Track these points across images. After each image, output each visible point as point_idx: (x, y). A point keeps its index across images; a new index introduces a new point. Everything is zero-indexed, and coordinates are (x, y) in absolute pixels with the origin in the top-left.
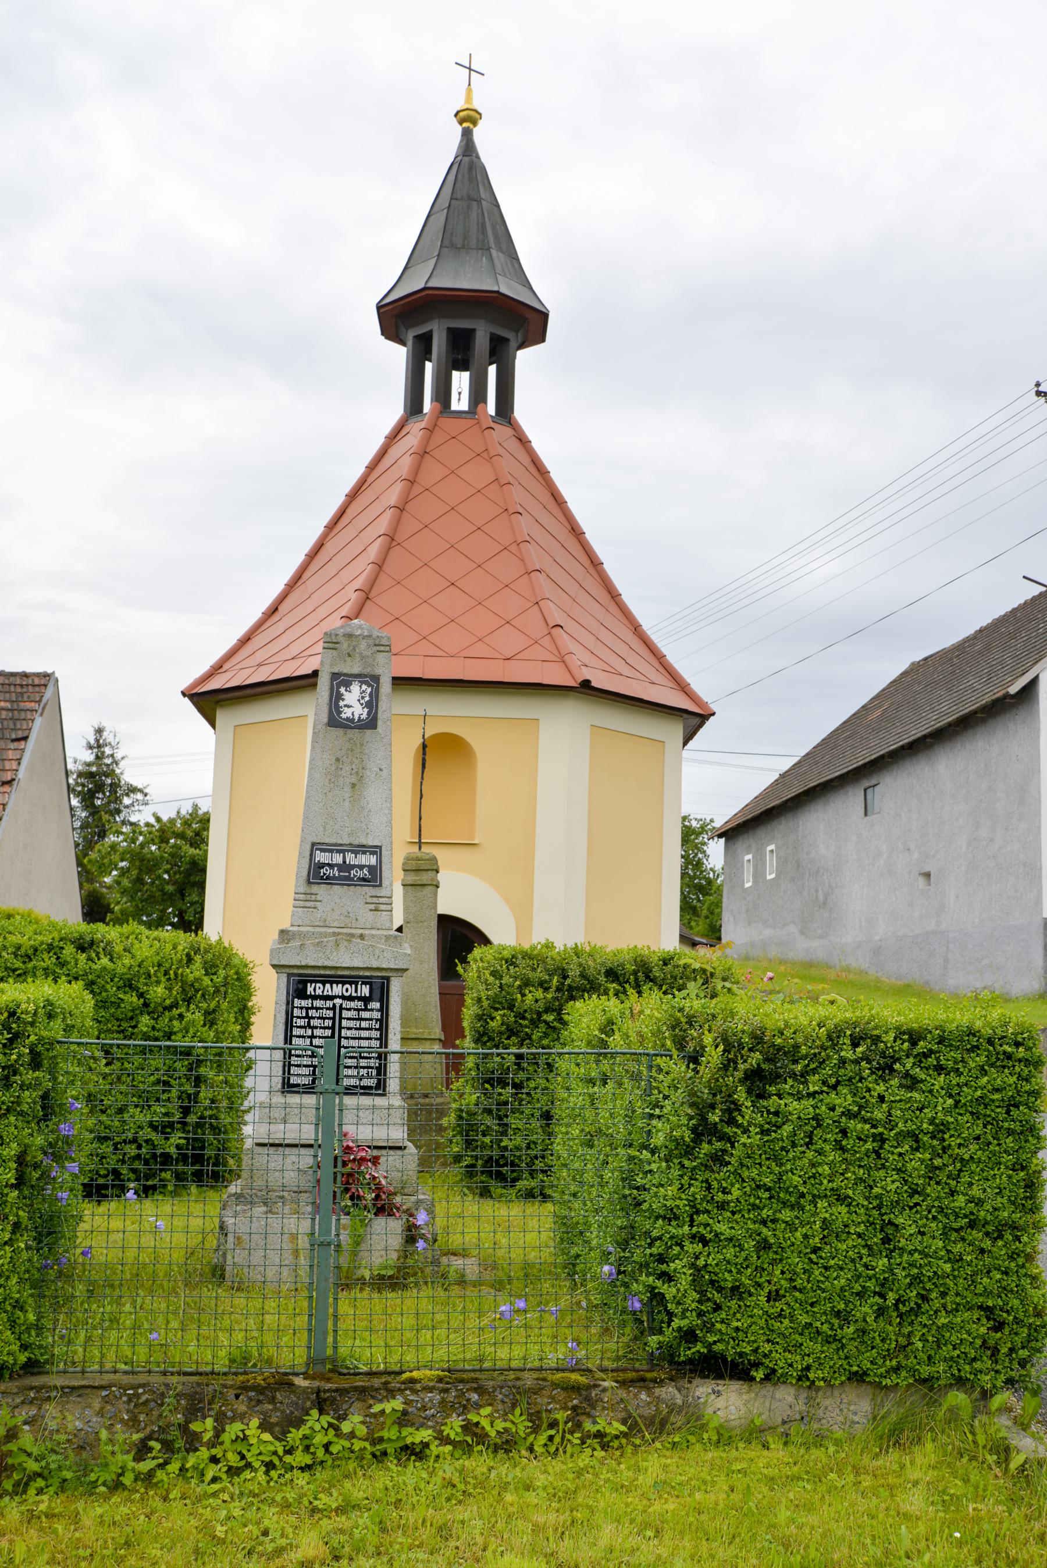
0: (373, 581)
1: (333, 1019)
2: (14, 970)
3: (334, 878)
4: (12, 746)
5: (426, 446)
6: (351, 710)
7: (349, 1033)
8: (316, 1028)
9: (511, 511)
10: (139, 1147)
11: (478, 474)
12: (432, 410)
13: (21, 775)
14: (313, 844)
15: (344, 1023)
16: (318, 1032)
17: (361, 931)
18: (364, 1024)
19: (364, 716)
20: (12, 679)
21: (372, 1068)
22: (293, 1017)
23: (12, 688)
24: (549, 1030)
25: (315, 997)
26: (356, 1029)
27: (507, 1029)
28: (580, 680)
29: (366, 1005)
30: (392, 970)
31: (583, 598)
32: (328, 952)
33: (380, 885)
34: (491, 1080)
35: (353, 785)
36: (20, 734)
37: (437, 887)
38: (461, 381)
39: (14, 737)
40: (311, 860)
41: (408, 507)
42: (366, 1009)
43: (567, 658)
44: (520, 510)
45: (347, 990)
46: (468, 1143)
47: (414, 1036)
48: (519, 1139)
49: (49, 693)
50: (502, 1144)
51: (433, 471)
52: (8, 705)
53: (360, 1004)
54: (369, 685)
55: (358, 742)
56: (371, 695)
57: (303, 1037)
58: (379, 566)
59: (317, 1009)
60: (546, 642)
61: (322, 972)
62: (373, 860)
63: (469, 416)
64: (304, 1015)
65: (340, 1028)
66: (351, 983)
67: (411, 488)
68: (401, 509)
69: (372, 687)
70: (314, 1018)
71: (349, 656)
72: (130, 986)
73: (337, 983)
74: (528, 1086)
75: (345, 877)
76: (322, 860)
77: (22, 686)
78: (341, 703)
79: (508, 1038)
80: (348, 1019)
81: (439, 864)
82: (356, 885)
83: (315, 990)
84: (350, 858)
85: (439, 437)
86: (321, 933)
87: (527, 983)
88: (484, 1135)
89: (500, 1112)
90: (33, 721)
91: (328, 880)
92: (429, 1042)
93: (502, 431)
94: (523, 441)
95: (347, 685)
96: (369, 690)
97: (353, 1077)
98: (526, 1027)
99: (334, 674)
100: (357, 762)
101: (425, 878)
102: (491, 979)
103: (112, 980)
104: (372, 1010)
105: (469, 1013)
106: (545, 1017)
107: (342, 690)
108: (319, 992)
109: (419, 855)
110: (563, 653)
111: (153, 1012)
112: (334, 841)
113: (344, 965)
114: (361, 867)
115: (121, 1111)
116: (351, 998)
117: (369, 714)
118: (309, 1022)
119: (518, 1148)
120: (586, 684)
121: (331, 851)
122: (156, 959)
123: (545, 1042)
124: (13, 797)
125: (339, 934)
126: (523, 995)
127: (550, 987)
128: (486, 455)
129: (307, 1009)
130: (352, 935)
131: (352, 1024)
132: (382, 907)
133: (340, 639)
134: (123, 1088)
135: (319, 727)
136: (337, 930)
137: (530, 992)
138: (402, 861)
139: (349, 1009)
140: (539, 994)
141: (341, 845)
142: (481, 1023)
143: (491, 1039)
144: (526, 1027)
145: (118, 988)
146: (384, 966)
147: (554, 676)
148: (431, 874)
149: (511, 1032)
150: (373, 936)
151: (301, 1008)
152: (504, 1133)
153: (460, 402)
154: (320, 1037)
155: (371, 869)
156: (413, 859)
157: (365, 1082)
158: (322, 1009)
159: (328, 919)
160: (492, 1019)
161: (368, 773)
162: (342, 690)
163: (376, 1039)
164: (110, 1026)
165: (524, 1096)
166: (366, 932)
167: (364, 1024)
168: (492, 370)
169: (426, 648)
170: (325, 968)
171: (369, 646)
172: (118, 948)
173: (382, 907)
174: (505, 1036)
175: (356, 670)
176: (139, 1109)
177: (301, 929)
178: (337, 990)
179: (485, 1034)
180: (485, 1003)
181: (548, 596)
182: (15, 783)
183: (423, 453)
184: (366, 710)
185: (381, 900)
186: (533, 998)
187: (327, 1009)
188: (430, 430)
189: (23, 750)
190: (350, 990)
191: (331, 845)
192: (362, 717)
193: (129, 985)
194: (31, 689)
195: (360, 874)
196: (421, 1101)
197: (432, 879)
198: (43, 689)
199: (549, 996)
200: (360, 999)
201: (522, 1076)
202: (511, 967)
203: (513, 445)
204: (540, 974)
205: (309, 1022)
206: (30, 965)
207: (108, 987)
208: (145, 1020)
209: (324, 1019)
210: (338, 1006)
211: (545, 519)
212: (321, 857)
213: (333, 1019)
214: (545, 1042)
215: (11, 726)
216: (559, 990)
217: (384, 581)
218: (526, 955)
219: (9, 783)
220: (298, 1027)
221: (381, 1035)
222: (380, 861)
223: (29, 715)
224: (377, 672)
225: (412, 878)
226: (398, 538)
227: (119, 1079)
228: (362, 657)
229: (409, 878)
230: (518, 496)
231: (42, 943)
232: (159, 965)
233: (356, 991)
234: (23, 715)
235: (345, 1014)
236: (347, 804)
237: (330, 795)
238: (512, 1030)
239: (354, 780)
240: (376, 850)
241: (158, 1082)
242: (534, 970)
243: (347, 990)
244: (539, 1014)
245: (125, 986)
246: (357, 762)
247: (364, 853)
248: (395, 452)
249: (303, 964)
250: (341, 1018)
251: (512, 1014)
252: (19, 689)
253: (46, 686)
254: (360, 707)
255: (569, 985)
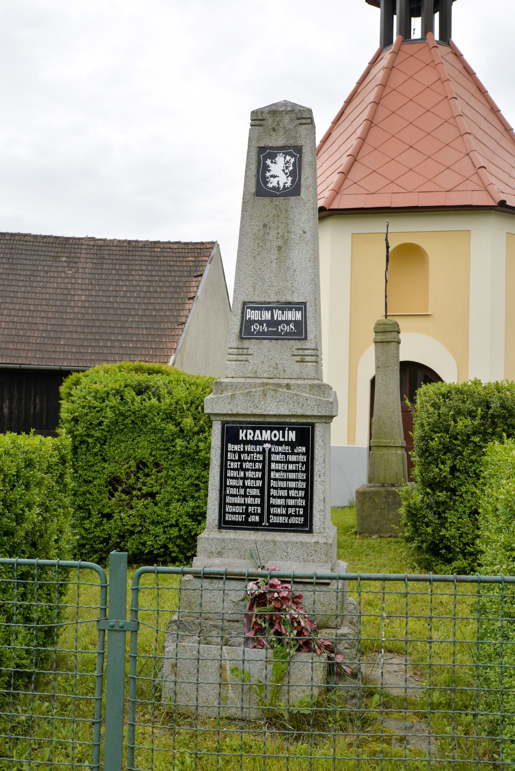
0: (359, 149)
1: (263, 462)
2: (95, 408)
3: (263, 333)
4: (195, 279)
5: (393, 63)
6: (276, 179)
7: (277, 475)
8: (248, 470)
9: (449, 97)
10: (180, 530)
11: (427, 77)
12: (397, 41)
13: (199, 294)
14: (244, 303)
15: (273, 466)
16: (249, 474)
17: (288, 381)
18: (291, 467)
19: (289, 184)
20: (196, 246)
21: (300, 507)
22: (227, 460)
23: (196, 250)
24: (477, 448)
25: (246, 442)
26: (284, 471)
27: (444, 447)
28: (498, 200)
29: (292, 449)
30: (315, 417)
31: (500, 151)
32: (256, 402)
33: (306, 339)
34: (433, 485)
35: (280, 248)
36: (199, 273)
37: (399, 343)
38: (416, 23)
39: (195, 275)
40: (242, 317)
41: (381, 102)
42: (293, 453)
43: (489, 187)
44: (456, 96)
45: (275, 436)
46: (416, 530)
47: (384, 445)
48: (453, 530)
49: (214, 252)
50: (441, 533)
51: (398, 78)
52: (193, 259)
53: (287, 449)
54: (292, 156)
55: (283, 208)
56: (294, 164)
57: (236, 478)
58: (363, 139)
59: (249, 453)
60: (475, 178)
61: (252, 419)
62: (298, 316)
63: (421, 41)
64: (237, 458)
65: (270, 470)
66: (278, 429)
67: (383, 90)
68: (377, 103)
69: (295, 157)
70: (245, 461)
71: (274, 130)
72: (171, 418)
73: (266, 429)
74: (461, 491)
75: (273, 331)
76: (252, 318)
77: (200, 249)
78: (268, 174)
79: (445, 454)
80: (277, 462)
81: (400, 327)
82: (283, 339)
83: (246, 435)
84: (278, 315)
85: (402, 56)
86: (251, 384)
87: (459, 412)
88: (428, 526)
89: (440, 509)
90: (205, 266)
91: (261, 336)
92: (394, 449)
93: (443, 50)
94: (458, 55)
95: (273, 157)
96: (293, 160)
97: (282, 515)
98: (458, 445)
99: (260, 148)
100: (282, 226)
101: (389, 337)
102: (431, 410)
103: (158, 414)
104: (298, 454)
105: (416, 434)
106: (473, 438)
107: (268, 162)
108: (250, 437)
109: (385, 321)
110: (486, 184)
111: (185, 436)
112: (262, 299)
113: (271, 413)
114: (288, 322)
115: (168, 504)
116: (279, 443)
117: (293, 182)
118: (241, 465)
119: (453, 537)
120: (503, 203)
121: (260, 309)
122: (189, 399)
123: (473, 457)
124: (194, 305)
125: (267, 384)
126: (456, 422)
127: (476, 416)
128: (433, 64)
129: (240, 453)
130: (279, 385)
131: (280, 466)
132: (308, 358)
133: (265, 116)
134: (169, 489)
135: (248, 197)
136: (265, 381)
137: (461, 420)
138: (374, 326)
139: (277, 453)
140: (468, 421)
141: (269, 303)
142: (424, 442)
143: (431, 454)
144: (458, 445)
145: (163, 420)
146: (308, 413)
147: (480, 199)
148: (394, 334)
149: (447, 449)
150: (298, 385)
151: (234, 452)
152: (442, 525)
153: (417, 33)
154: (252, 479)
155: (297, 323)
156: (381, 324)
157: (293, 520)
158: (253, 453)
159: (259, 370)
160: (432, 439)
161: (293, 236)
162: (268, 162)
163: (302, 480)
164: (158, 445)
165: (457, 498)
166: (292, 382)
167: (291, 467)
168: (437, 16)
169: (394, 188)
170: (254, 415)
171: (291, 120)
172: (164, 391)
173: (308, 358)
174: (442, 453)
175: (280, 143)
176: (179, 503)
177: (234, 380)
178: (266, 435)
179: (426, 451)
180: (427, 428)
181: (475, 149)
182: (195, 298)
183: (391, 68)
184: (290, 179)
185: (307, 352)
186: (463, 424)
187: (258, 453)
188: (396, 53)
189: (200, 281)
190: (278, 435)
191: (260, 303)
192: (287, 185)
193: (169, 417)
194: (205, 250)
195: (287, 329)
196: (389, 489)
197: (394, 338)
198: (211, 250)
199: (476, 423)
200: (287, 443)
201: (456, 482)
202: (447, 400)
203: (451, 58)
204: (469, 405)
205: (241, 465)
206: (104, 404)
207: (156, 419)
208: (179, 442)
209: (255, 462)
210: (267, 450)
211: (473, 102)
212: (252, 315)
213: (263, 462)
214: (473, 457)
215: (195, 269)
216: (483, 417)
217: (366, 149)
218: (459, 391)
219: (192, 298)
220: (231, 469)
221: (307, 476)
222: (305, 316)
223: (203, 264)
224: (300, 143)
225: (381, 337)
226: (375, 121)
227: (166, 482)
228: (286, 131)
229: (379, 337)
230: (454, 88)
231: (112, 389)
232: (192, 403)
233: (284, 437)
234: (200, 263)
235: (274, 457)
236: (274, 265)
237: (258, 258)
238: (447, 448)
239: (280, 243)
240: (301, 307)
241: (192, 484)
242: (464, 402)
243: (275, 436)
244: (468, 436)
245: (167, 418)
246: (282, 226)
247: (290, 309)
248: (374, 72)
249: (234, 412)
250: (270, 461)
251: (448, 436)
252: (199, 251)
253: (212, 248)
254: (285, 176)
255: (492, 414)
